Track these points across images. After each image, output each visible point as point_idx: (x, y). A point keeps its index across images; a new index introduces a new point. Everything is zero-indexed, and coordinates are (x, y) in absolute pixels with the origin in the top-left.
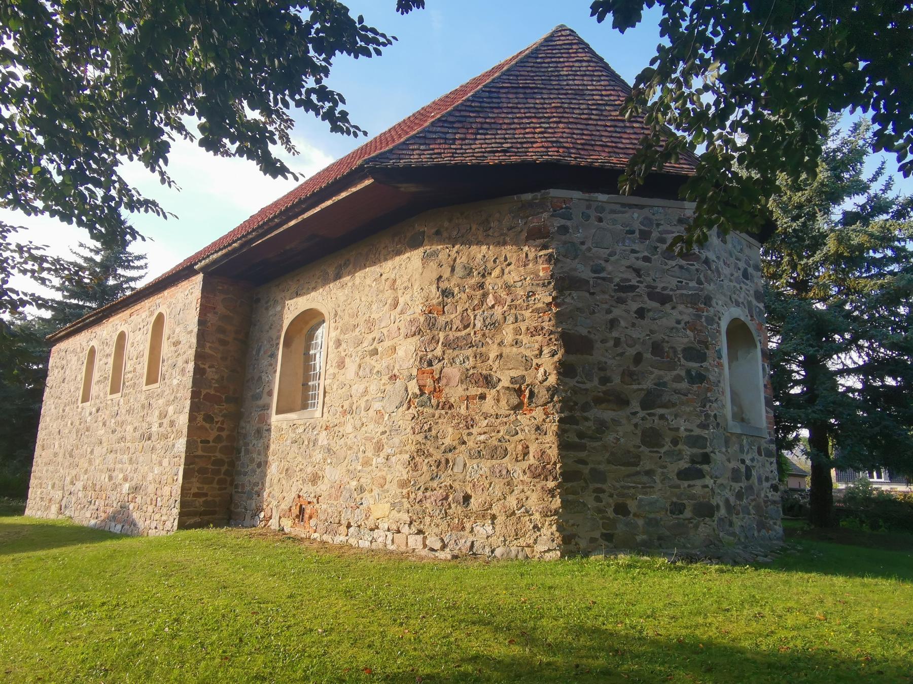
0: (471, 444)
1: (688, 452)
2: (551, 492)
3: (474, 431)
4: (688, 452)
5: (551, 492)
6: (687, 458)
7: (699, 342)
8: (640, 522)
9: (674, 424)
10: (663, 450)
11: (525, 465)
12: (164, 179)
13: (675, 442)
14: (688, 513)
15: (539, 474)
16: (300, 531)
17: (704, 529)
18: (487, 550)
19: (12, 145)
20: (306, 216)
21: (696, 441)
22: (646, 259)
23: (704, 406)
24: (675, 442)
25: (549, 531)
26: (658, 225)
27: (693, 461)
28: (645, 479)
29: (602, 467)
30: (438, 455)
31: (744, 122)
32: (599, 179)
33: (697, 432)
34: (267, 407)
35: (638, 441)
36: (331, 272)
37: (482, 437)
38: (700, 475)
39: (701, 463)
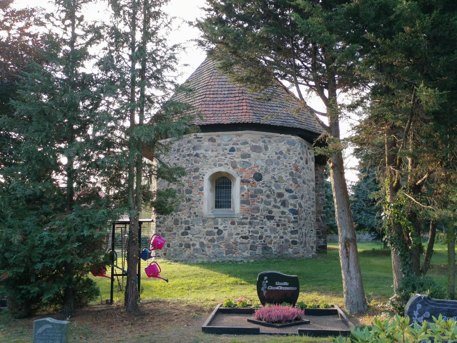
1: (184, 226)
4: (184, 226)
6: (184, 228)
7: (190, 187)
8: (172, 249)
9: (181, 217)
10: (178, 226)
12: (94, 57)
13: (181, 223)
14: (183, 247)
17: (188, 252)
21: (186, 222)
22: (178, 159)
23: (190, 210)
24: (181, 223)
26: (182, 145)
27: (186, 229)
28: (173, 236)
29: (164, 232)
31: (311, 70)
32: (206, 128)
33: (187, 219)
35: (173, 223)
38: (187, 234)
39: (188, 230)
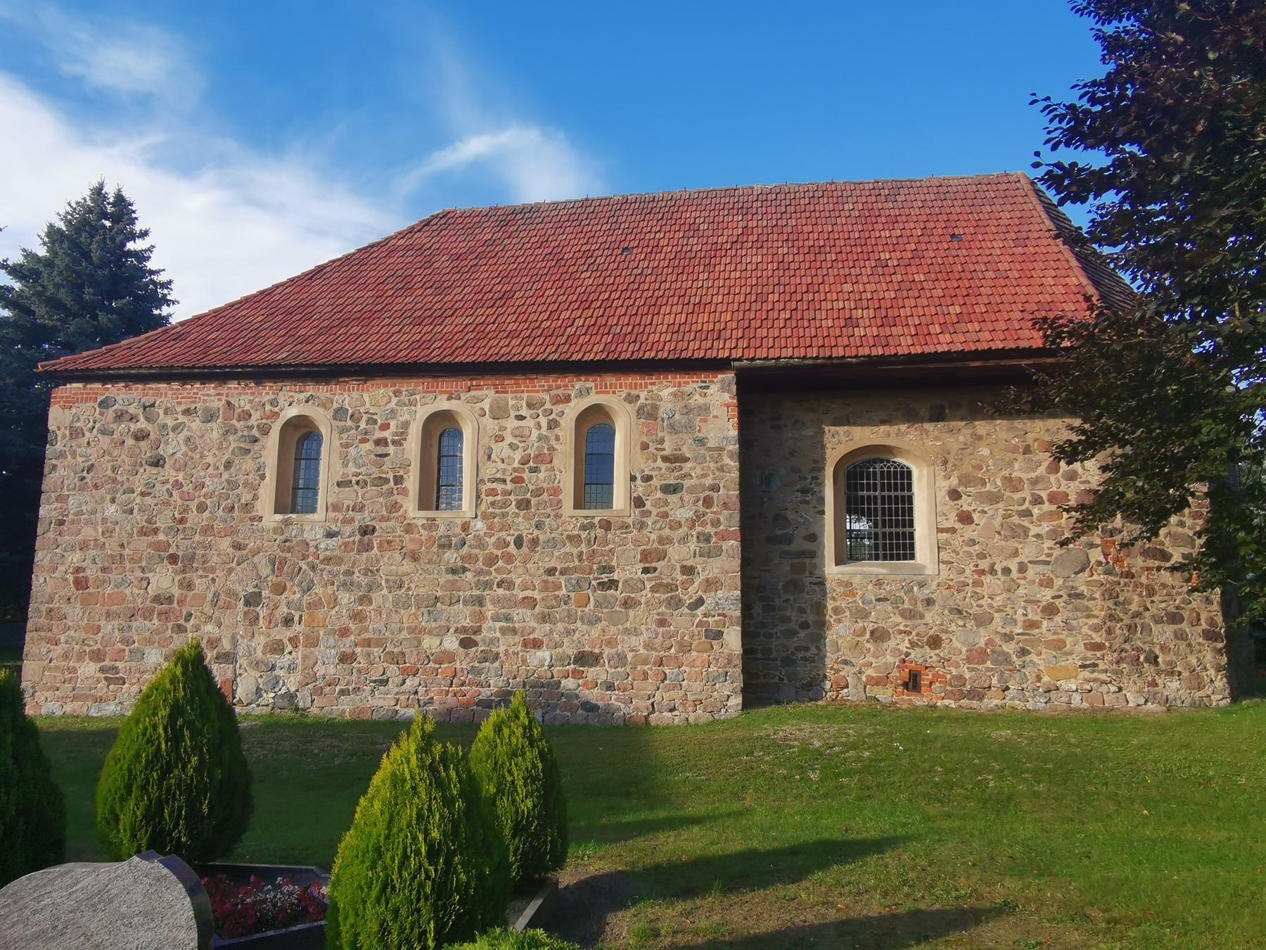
0: (1153, 610)
2: (1219, 651)
3: (1155, 598)
5: (1219, 651)
11: (1199, 629)
15: (1210, 636)
16: (920, 701)
18: (1179, 702)
19: (1171, 316)
20: (1003, 363)
25: (1221, 682)
30: (1127, 621)
34: (813, 555)
36: (924, 411)
37: (1163, 605)
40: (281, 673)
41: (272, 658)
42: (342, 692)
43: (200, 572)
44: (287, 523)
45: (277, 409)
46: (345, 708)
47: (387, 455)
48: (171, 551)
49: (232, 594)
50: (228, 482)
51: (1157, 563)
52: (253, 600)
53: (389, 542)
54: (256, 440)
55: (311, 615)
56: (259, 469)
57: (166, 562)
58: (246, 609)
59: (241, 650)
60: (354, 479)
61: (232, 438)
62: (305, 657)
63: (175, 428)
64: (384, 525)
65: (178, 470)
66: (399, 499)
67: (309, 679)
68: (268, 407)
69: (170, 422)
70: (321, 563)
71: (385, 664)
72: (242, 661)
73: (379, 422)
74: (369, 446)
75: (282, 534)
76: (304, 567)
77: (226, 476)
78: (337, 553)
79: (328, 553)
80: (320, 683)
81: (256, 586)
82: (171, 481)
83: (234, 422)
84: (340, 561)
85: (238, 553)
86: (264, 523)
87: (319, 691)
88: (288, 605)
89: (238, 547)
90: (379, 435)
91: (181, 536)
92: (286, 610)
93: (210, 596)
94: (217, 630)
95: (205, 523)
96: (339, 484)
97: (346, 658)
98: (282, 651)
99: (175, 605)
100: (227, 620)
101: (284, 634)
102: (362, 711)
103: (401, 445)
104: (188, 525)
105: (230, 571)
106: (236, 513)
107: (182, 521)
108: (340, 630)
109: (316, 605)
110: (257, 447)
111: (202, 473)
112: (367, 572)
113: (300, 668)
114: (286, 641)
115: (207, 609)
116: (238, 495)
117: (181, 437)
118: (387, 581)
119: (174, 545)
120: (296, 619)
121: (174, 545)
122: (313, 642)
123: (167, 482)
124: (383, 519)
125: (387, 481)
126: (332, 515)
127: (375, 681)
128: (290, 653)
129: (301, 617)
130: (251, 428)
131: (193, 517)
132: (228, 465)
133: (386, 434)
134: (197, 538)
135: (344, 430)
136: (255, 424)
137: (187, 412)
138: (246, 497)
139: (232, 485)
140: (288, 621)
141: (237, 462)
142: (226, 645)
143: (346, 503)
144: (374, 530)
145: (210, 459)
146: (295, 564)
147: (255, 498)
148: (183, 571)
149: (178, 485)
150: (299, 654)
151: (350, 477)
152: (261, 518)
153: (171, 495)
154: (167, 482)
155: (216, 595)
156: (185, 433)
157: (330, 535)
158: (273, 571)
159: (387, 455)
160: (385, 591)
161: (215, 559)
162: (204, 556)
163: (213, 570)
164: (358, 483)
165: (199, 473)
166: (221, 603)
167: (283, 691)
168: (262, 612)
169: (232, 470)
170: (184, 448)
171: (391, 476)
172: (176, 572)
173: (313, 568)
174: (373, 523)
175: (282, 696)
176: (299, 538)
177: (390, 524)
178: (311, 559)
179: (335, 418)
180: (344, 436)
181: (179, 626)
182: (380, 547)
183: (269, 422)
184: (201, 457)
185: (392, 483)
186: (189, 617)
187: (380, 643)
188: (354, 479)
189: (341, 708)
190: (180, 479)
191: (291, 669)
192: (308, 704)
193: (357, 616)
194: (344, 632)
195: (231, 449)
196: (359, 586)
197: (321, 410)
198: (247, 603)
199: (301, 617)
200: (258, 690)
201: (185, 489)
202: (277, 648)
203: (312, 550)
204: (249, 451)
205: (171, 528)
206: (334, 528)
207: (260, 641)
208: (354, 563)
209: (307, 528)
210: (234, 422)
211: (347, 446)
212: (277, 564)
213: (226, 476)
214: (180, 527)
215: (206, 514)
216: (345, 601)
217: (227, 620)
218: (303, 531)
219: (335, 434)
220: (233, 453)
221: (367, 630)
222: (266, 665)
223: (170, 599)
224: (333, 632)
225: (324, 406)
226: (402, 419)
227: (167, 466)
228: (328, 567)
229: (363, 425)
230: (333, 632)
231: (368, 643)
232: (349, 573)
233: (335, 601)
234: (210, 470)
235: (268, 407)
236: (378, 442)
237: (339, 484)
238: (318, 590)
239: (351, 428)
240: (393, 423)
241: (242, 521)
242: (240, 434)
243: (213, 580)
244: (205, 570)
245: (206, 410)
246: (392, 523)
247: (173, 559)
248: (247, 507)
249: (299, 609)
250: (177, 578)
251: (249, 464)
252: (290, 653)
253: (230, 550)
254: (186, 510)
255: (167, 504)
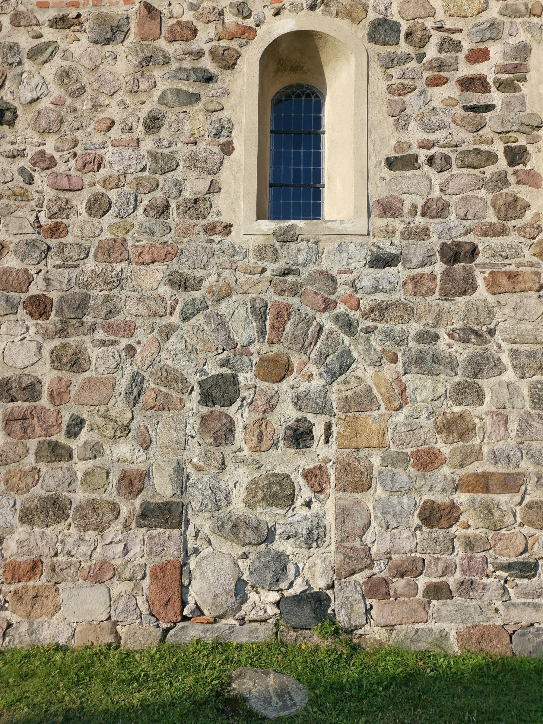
40: (286, 547)
41: (266, 515)
42: (438, 591)
43: (100, 335)
44: (286, 238)
45: (250, 22)
46: (446, 629)
47: (489, 108)
48: (34, 290)
49: (173, 379)
50: (154, 156)
51: (159, 338)
52: (219, 391)
53: (511, 276)
54: (209, 79)
55: (350, 424)
56: (218, 135)
57: (22, 313)
58: (205, 410)
59: (195, 499)
60: (423, 155)
61: (158, 73)
62: (343, 514)
63: (33, 54)
64: (495, 241)
65: (47, 131)
66: (523, 192)
67: (353, 560)
68: (230, 19)
69: (24, 41)
70: (366, 316)
71: (527, 530)
72: (200, 522)
73: (466, 46)
74: (450, 90)
75: (276, 258)
76: (329, 325)
77: (148, 144)
78: (399, 296)
79: (380, 297)
80: (380, 570)
81: (226, 363)
82: (31, 152)
83: (162, 43)
84: (406, 312)
85: (184, 297)
86: (236, 237)
87: (378, 589)
88: (299, 401)
89: (182, 283)
90: (466, 70)
91: (53, 260)
92: (293, 414)
93: (123, 383)
94: (141, 455)
95: (106, 235)
96: (391, 164)
97: (435, 516)
98: (291, 498)
99: (44, 401)
100: (163, 432)
101: (292, 464)
102: (487, 634)
103: (516, 89)
104: (69, 239)
105: (168, 331)
106: (174, 217)
107: (56, 230)
108: (417, 455)
109: (363, 401)
110: (212, 89)
111: (98, 138)
112: (468, 334)
113: (332, 536)
114: (298, 478)
115: (118, 408)
116: (176, 183)
117: (50, 70)
118: (515, 353)
119: (39, 280)
120: (319, 430)
121: (39, 280)
122: (357, 480)
123: (21, 154)
124: (489, 231)
125: (491, 158)
126: (379, 223)
127: (508, 567)
128: (308, 504)
129: (328, 427)
130: (199, 54)
131: (79, 223)
132: (153, 123)
133: (482, 69)
134: (90, 264)
135: (389, 63)
136: (207, 48)
137: (60, 22)
138: (195, 185)
139: (164, 163)
140: (300, 436)
141: (170, 116)
142: (162, 488)
143: (408, 200)
144: (474, 251)
145: (114, 111)
146: (308, 320)
147: (214, 188)
148: (62, 332)
149: (46, 162)
150: (328, 508)
151: (414, 150)
152: (227, 228)
153: (30, 181)
154: (21, 154)
155: (137, 381)
156: (57, 62)
157: (381, 261)
158: (262, 332)
159: (489, 108)
160: (510, 375)
161: (133, 306)
162: (107, 300)
163: (129, 329)
164: (431, 161)
165: (91, 138)
166: (148, 398)
167: (298, 588)
168: (241, 416)
169: (164, 133)
170: (56, 91)
171: (498, 148)
172: (46, 335)
173: (349, 327)
174: (471, 238)
175: (297, 599)
176: (312, 268)
177: (507, 240)
178: (341, 308)
179: (372, 37)
180: (396, 72)
181: (54, 447)
182: (493, 286)
183: (234, 44)
184: (96, 107)
185: (503, 163)
186: (75, 426)
187: (511, 483)
188: (423, 155)
189: (436, 627)
190: (50, 148)
191: (313, 538)
192: (359, 617)
193: (456, 428)
194: (428, 460)
195: (157, 94)
196: (452, 364)
197: (344, 23)
198: (207, 398)
199: (328, 427)
200: (240, 588)
201: (61, 168)
202: (279, 492)
203: (342, 291)
204: (198, 98)
205: (32, 244)
206: (387, 248)
207: (239, 479)
208: (439, 317)
209: (328, 246)
210: (162, 43)
211: (403, 90)
212: (268, 319)
213: (148, 144)
214: (53, 242)
215: (109, 219)
216: (425, 395)
217: (163, 432)
218: (319, 253)
219: (377, 69)
220: (162, 100)
221: (478, 456)
222: (256, 529)
223: (32, 390)
224: (400, 460)
225: (349, 15)
226: (513, 41)
227: (20, 124)
228: (381, 326)
229: (432, 52)
230: (400, 460)
231: (483, 483)
232: (428, 337)
233: (401, 396)
234: (116, 133)
235: (230, 19)
236: (469, 84)
237: (391, 164)
238: (363, 371)
239: (408, 58)
240: (496, 51)
241: (187, 232)
242: (175, 65)
243: (130, 350)
244: (109, 329)
245: (102, 20)
246: (513, 239)
247: (39, 307)
248: (196, 206)
249: (324, 409)
250: (48, 346)
251: (197, 120)
252: (308, 504)
253: (166, 290)
254: (65, 209)
255: (22, 196)
